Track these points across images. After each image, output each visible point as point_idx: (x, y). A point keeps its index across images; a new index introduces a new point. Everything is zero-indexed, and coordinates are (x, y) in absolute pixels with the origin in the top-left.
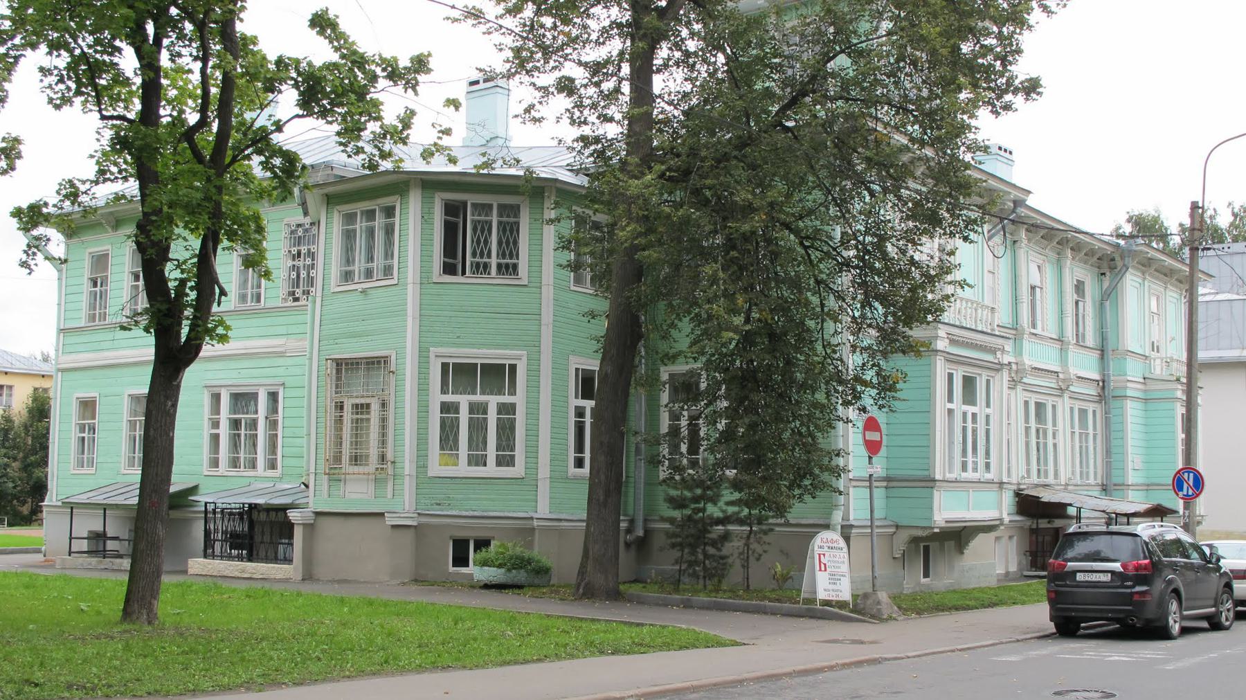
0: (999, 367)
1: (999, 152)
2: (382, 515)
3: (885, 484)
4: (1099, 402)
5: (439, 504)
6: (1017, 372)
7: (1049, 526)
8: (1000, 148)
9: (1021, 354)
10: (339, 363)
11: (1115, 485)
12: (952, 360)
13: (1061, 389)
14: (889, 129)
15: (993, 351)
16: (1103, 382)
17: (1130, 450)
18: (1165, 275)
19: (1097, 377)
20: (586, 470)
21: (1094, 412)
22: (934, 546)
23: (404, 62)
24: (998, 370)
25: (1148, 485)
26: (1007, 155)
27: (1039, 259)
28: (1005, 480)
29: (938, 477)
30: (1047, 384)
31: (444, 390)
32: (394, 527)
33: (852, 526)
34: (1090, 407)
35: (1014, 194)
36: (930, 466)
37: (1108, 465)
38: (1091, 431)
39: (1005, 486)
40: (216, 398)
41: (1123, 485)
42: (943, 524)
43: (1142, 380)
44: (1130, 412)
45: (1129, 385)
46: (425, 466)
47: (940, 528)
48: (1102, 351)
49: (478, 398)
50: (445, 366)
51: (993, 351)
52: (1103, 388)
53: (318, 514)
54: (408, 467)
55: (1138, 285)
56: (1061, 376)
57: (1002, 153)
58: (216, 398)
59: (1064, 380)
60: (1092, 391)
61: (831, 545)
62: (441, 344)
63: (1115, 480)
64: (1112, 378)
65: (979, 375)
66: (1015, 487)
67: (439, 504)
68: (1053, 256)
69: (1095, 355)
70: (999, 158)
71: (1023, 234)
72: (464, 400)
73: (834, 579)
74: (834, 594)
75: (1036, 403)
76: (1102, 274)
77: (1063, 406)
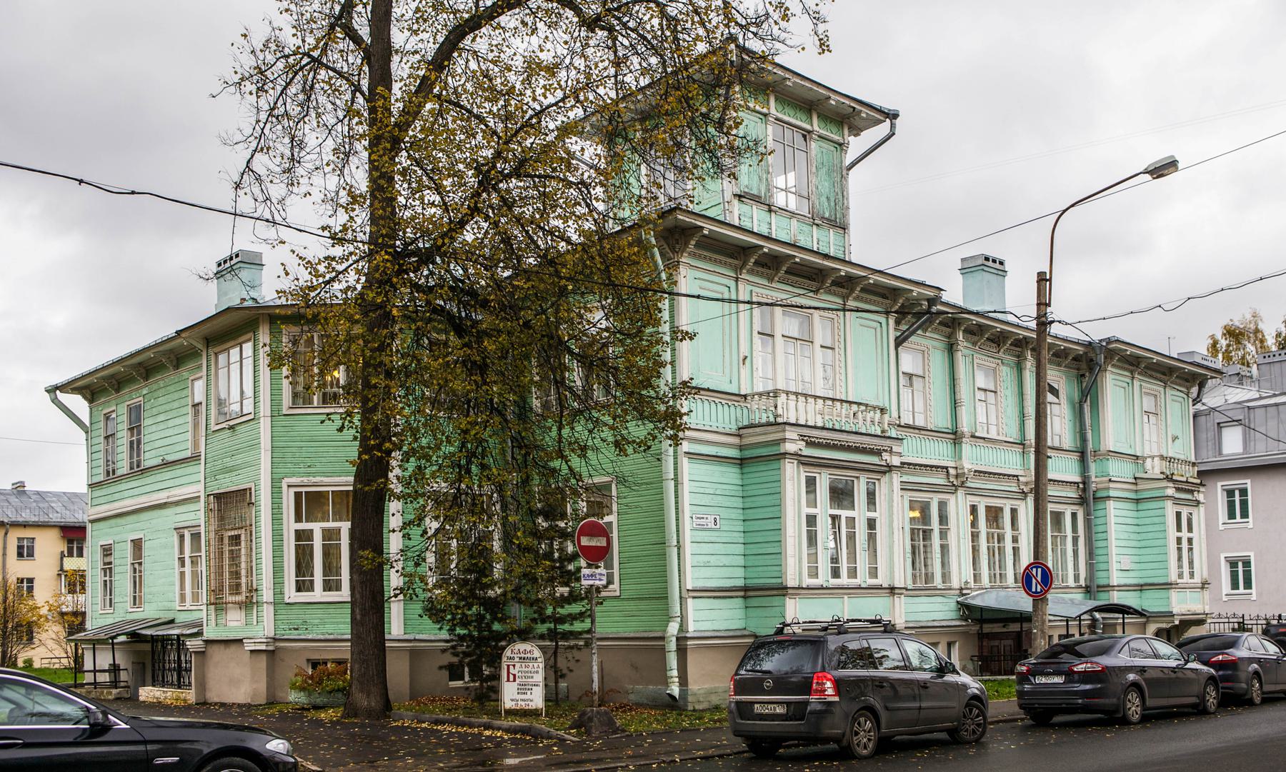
1: (986, 263)
2: (240, 641)
3: (742, 594)
4: (1080, 504)
6: (957, 476)
7: (1005, 630)
8: (987, 259)
9: (960, 458)
10: (219, 497)
11: (1098, 587)
12: (804, 461)
13: (1023, 492)
15: (878, 453)
16: (1084, 483)
17: (1114, 551)
19: (1078, 479)
20: (345, 594)
21: (1074, 515)
24: (884, 473)
25: (1142, 586)
26: (997, 265)
27: (991, 363)
30: (1003, 488)
31: (298, 519)
32: (251, 651)
33: (687, 638)
34: (1068, 511)
35: (931, 293)
37: (1091, 567)
39: (897, 591)
40: (182, 537)
41: (1108, 586)
43: (1134, 481)
45: (1112, 485)
46: (282, 593)
49: (331, 524)
50: (298, 495)
51: (878, 453)
52: (1084, 490)
53: (207, 642)
54: (267, 594)
55: (1181, 400)
57: (990, 263)
58: (182, 537)
60: (1072, 493)
61: (523, 655)
62: (293, 475)
63: (1102, 582)
64: (1093, 479)
65: (857, 477)
68: (1010, 359)
69: (1075, 457)
70: (986, 269)
71: (960, 336)
72: (317, 528)
73: (523, 688)
77: (958, 506)
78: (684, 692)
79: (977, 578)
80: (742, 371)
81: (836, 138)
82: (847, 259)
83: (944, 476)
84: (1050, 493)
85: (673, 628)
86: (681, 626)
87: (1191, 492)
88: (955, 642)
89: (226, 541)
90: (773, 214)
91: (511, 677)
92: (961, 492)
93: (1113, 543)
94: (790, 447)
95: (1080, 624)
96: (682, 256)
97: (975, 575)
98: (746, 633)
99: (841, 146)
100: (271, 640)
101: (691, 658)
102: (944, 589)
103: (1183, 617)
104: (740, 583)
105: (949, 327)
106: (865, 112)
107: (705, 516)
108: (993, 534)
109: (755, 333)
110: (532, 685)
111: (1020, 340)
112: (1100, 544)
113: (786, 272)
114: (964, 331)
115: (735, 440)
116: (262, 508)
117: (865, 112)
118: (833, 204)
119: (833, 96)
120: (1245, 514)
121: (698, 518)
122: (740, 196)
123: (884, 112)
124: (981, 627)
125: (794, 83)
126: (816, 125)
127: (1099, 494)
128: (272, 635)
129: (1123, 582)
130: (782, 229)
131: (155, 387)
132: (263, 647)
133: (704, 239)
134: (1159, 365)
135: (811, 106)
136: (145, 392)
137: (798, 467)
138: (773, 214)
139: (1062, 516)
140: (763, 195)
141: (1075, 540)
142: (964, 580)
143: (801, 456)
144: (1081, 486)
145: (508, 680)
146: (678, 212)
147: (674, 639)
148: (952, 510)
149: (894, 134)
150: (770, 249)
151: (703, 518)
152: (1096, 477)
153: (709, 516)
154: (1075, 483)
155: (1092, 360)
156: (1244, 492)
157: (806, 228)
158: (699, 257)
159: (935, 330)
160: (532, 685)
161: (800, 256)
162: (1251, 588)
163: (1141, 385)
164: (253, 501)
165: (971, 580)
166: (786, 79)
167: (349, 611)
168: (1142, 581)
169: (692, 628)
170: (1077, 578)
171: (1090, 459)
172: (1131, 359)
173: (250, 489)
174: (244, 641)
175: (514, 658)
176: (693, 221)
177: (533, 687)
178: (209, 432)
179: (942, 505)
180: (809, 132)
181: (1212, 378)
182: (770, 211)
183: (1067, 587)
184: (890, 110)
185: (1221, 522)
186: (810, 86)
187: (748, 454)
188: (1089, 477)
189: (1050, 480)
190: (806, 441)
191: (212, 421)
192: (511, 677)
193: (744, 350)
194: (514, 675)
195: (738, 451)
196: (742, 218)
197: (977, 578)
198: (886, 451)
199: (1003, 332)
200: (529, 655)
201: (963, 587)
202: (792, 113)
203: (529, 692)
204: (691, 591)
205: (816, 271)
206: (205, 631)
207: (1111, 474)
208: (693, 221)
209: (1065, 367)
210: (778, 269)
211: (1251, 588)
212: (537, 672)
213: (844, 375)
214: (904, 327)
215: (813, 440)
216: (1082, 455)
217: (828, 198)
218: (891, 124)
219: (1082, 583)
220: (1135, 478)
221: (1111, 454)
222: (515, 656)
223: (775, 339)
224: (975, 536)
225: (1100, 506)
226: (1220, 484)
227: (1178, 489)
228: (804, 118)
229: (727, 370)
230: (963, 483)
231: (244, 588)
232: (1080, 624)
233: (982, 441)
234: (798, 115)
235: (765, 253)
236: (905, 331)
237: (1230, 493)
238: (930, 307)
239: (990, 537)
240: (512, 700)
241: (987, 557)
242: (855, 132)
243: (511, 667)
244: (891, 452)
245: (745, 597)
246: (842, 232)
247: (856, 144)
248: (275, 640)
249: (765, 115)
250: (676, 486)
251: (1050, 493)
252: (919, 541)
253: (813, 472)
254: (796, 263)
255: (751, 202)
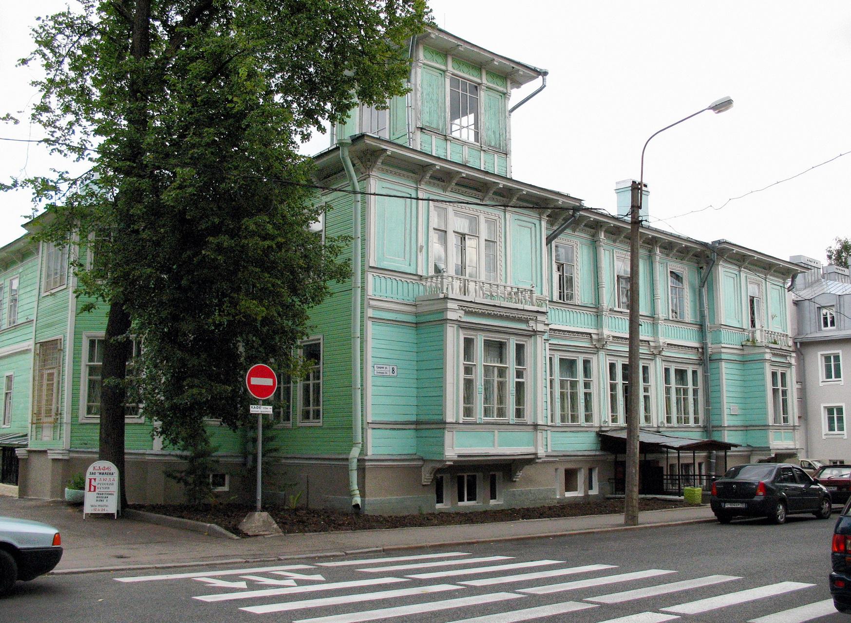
0: (532, 333)
2: (45, 452)
3: (413, 426)
4: (699, 364)
5: (86, 444)
6: (599, 340)
10: (42, 344)
13: (653, 354)
14: (201, 149)
16: (703, 348)
17: (725, 400)
18: (765, 268)
19: (696, 345)
22: (499, 475)
23: (5, 116)
24: (531, 336)
25: (747, 427)
28: (540, 422)
29: (449, 420)
32: (54, 460)
33: (364, 460)
36: (443, 413)
37: (707, 412)
38: (690, 386)
41: (721, 426)
42: (456, 458)
43: (741, 347)
44: (724, 371)
45: (723, 350)
46: (77, 417)
47: (454, 461)
48: (701, 325)
52: (703, 353)
53: (30, 452)
54: (66, 418)
55: (734, 276)
56: (652, 344)
59: (655, 347)
60: (693, 356)
61: (102, 471)
63: (715, 423)
64: (709, 345)
66: (598, 430)
67: (86, 444)
69: (695, 328)
73: (101, 497)
74: (100, 508)
75: (643, 366)
76: (701, 268)
78: (363, 501)
79: (669, 420)
80: (420, 257)
81: (501, 89)
82: (508, 177)
83: (589, 341)
84: (641, 351)
85: (355, 453)
86: (362, 450)
87: (785, 356)
88: (595, 468)
89: (45, 377)
90: (449, 143)
91: (92, 488)
92: (602, 354)
93: (725, 394)
94: (768, 356)
95: (694, 455)
96: (372, 170)
97: (667, 417)
98: (414, 457)
99: (505, 95)
100: (67, 452)
101: (368, 476)
102: (587, 427)
103: (778, 451)
104: (413, 418)
105: (593, 228)
106: (522, 72)
107: (385, 366)
108: (680, 389)
109: (431, 229)
110: (108, 494)
111: (649, 239)
112: (714, 395)
113: (584, 226)
114: (605, 231)
115: (413, 309)
116: (67, 353)
117: (522, 72)
118: (498, 136)
119: (496, 59)
120: (838, 375)
121: (379, 367)
122: (422, 129)
123: (537, 71)
124: (616, 457)
125: (465, 48)
126: (485, 80)
127: (713, 357)
128: (68, 448)
129: (732, 423)
130: (453, 153)
131: (27, 267)
132: (60, 457)
133: (462, 179)
134: (529, 195)
135: (481, 66)
136: (21, 270)
137: (458, 331)
138: (449, 143)
139: (685, 374)
140: (441, 127)
141: (695, 392)
142: (603, 420)
143: (460, 321)
144: (700, 350)
145: (90, 490)
146: (365, 138)
147: (356, 460)
148: (594, 365)
149: (545, 86)
150: (441, 166)
151: (383, 368)
152: (712, 344)
153: (388, 367)
154: (695, 348)
155: (708, 257)
156: (837, 358)
157: (475, 153)
158: (774, 276)
159: (582, 231)
160: (108, 494)
161: (465, 172)
162: (843, 430)
163: (746, 277)
164: (62, 348)
165: (665, 421)
166: (519, 70)
167: (98, 431)
168: (747, 424)
169: (371, 452)
170: (696, 420)
171: (708, 330)
172: (439, 175)
173: (61, 339)
174: (48, 451)
175: (95, 474)
176: (378, 145)
177: (109, 496)
178: (40, 298)
179: (586, 363)
180: (479, 84)
181: (802, 272)
182: (446, 140)
183: (689, 427)
184: (541, 70)
185: (821, 380)
186: (478, 51)
187: (422, 319)
188: (706, 344)
189: (642, 341)
190: (465, 311)
191: (42, 290)
192: (92, 488)
193: (422, 241)
194: (95, 487)
195: (415, 317)
196: (423, 145)
197: (669, 420)
198: (532, 319)
199: (654, 237)
200: (107, 471)
201: (602, 425)
202: (466, 70)
203: (105, 500)
204: (371, 423)
205: (482, 185)
206: (29, 444)
207: (723, 342)
208: (378, 145)
209: (687, 261)
210: (450, 182)
211: (843, 430)
212: (113, 484)
213: (503, 261)
214: (555, 228)
215: (470, 310)
216: (701, 327)
217: (494, 132)
218: (543, 79)
219: (701, 424)
220: (742, 346)
221: (722, 327)
222: (97, 472)
223: (448, 234)
224: (668, 390)
225: (714, 365)
226: (820, 353)
227: (774, 355)
228: (475, 73)
229: (407, 256)
230: (603, 345)
231: (53, 413)
232: (694, 455)
233: (620, 314)
234: (435, 57)
235: (438, 169)
236: (556, 231)
237: (827, 358)
238: (574, 213)
239: (678, 390)
240: (92, 506)
241: (675, 405)
242: (517, 85)
243: (93, 480)
244: (536, 320)
245: (416, 430)
246: (504, 156)
247: (517, 94)
248: (70, 451)
249: (444, 71)
250: (362, 343)
251: (641, 351)
252: (567, 389)
253: (470, 334)
254: (463, 177)
255: (431, 133)
